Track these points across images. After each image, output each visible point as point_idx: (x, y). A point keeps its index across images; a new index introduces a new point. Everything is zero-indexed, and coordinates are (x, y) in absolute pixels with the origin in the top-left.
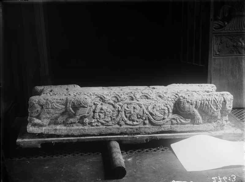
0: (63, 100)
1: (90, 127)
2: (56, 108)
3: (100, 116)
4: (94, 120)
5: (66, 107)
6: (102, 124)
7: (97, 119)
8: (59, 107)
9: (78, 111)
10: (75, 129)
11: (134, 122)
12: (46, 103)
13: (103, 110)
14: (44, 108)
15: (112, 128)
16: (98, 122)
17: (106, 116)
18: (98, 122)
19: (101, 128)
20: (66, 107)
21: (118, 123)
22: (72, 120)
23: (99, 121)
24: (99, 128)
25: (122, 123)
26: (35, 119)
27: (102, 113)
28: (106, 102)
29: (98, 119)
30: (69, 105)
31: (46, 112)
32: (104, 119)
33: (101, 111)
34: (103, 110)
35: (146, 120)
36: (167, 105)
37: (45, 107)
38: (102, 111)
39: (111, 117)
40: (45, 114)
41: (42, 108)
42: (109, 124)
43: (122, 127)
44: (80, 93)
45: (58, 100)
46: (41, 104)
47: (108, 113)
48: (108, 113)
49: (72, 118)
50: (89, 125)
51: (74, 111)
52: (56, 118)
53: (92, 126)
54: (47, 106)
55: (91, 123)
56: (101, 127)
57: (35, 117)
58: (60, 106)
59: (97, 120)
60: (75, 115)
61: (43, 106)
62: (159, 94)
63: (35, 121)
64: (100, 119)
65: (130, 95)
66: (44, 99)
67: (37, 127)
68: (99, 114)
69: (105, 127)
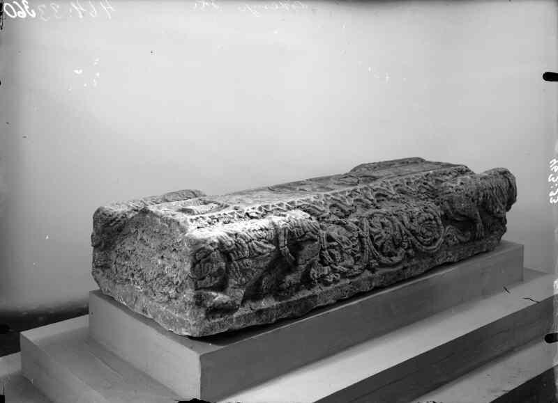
0: (267, 230)
1: (325, 289)
2: (260, 254)
3: (332, 256)
4: (326, 268)
5: (278, 247)
6: (344, 275)
7: (330, 264)
8: (265, 251)
9: (301, 253)
10: (298, 301)
11: (392, 258)
12: (236, 245)
13: (334, 240)
14: (233, 258)
15: (361, 281)
16: (334, 271)
17: (344, 255)
18: (334, 271)
19: (342, 287)
20: (278, 247)
21: (368, 267)
22: (290, 278)
23: (336, 269)
24: (340, 288)
25: (374, 263)
26: (214, 294)
27: (333, 247)
28: (326, 219)
29: (332, 265)
30: (283, 241)
31: (239, 269)
32: (343, 261)
33: (331, 244)
34: (334, 240)
35: (409, 248)
36: (426, 208)
37: (235, 256)
38: (335, 243)
39: (353, 255)
40: (237, 274)
41: (229, 260)
42: (355, 271)
43: (377, 273)
44: (279, 205)
45: (259, 233)
46: (227, 249)
47: (346, 246)
48: (346, 246)
49: (290, 274)
50: (319, 282)
51: (295, 257)
52: (258, 283)
53: (327, 284)
54: (240, 252)
55: (323, 276)
56: (343, 282)
57: (213, 289)
58: (268, 246)
59: (331, 267)
60: (296, 264)
61: (232, 255)
62: (400, 187)
63: (216, 299)
64: (335, 265)
65: (357, 197)
66: (230, 235)
67: (219, 315)
68: (329, 252)
69: (348, 281)
